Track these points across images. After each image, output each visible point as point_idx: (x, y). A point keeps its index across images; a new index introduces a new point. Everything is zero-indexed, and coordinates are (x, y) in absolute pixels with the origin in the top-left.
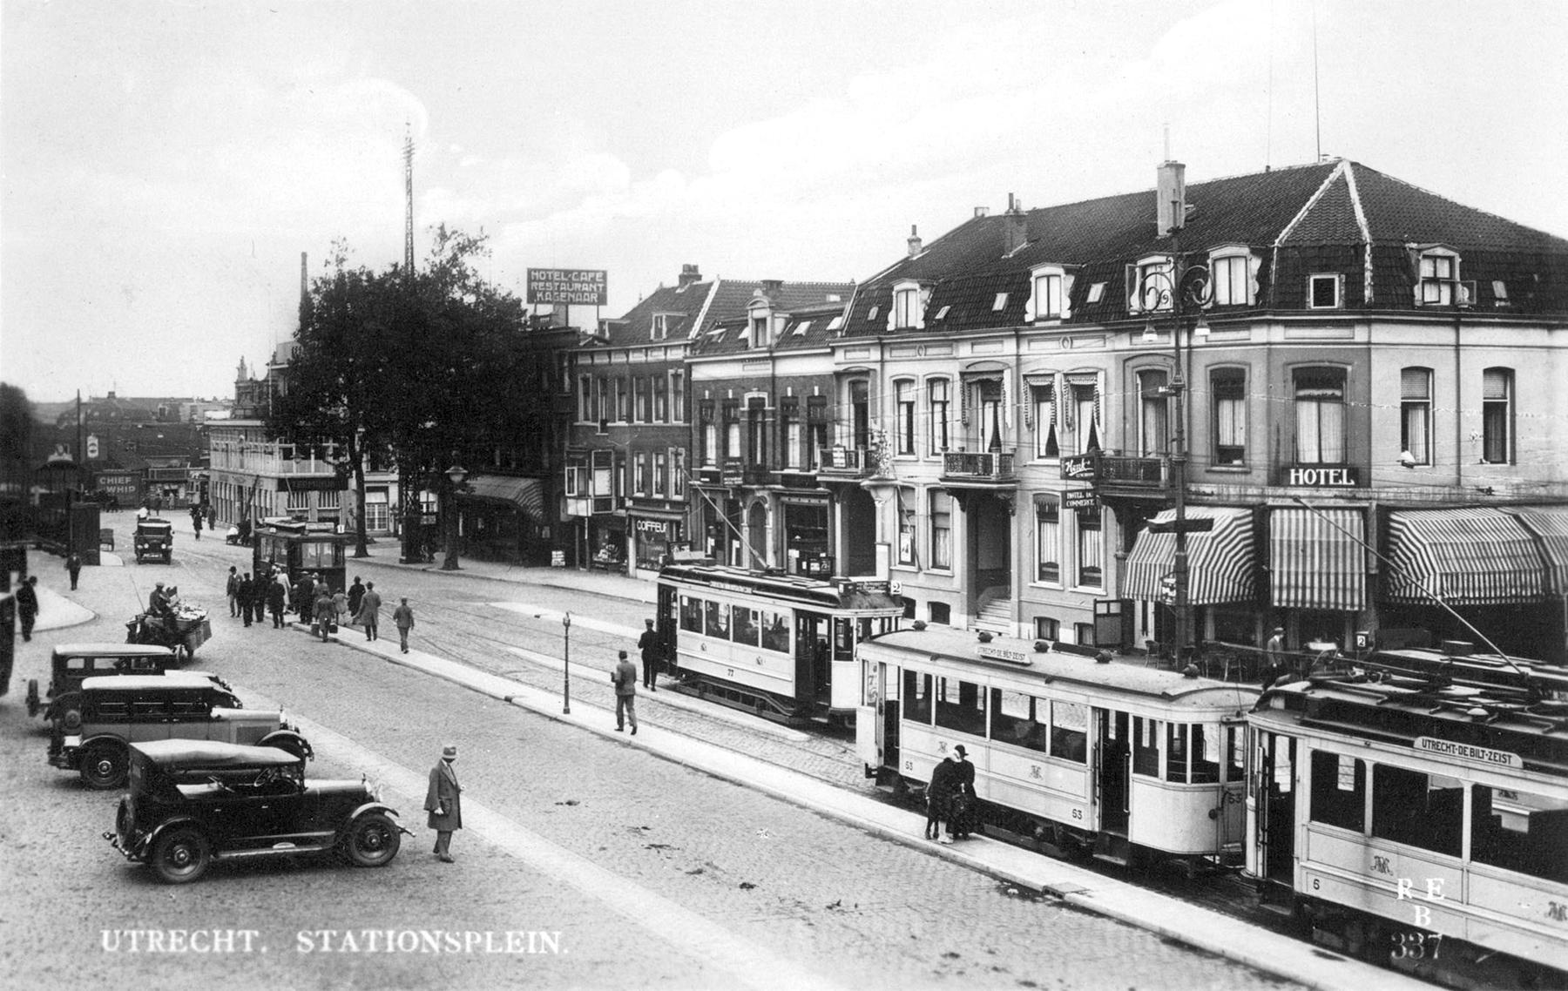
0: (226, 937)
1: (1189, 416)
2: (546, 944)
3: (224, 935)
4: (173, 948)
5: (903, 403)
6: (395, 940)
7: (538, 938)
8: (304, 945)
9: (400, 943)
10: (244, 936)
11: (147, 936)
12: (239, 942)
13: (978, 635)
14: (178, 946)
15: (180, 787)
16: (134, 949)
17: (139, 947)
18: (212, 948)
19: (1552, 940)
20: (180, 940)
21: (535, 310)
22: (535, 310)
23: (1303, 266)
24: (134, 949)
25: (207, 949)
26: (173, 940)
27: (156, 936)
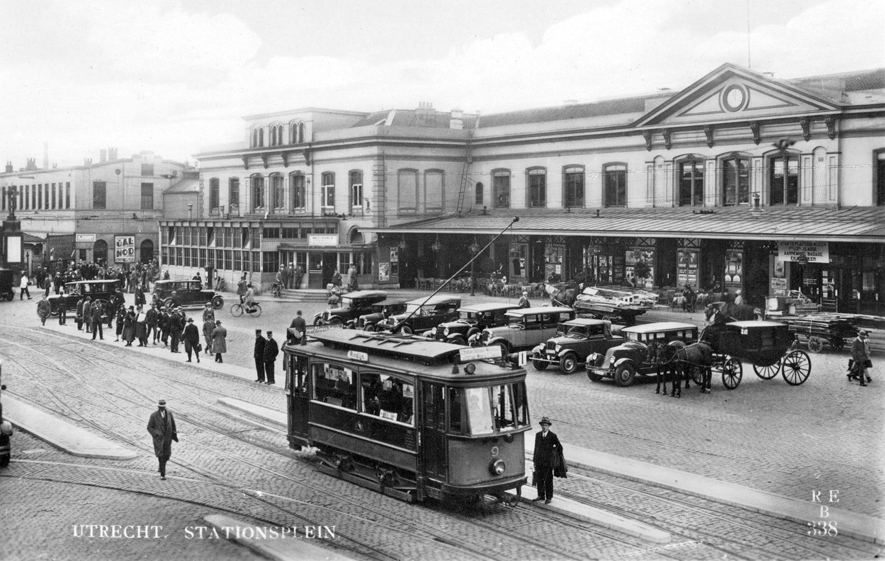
0: (144, 530)
1: (409, 139)
2: (259, 533)
3: (143, 528)
4: (113, 536)
5: (351, 209)
6: (241, 532)
7: (323, 528)
8: (188, 535)
9: (244, 533)
10: (89, 528)
11: (99, 529)
12: (152, 533)
13: (296, 316)
14: (116, 534)
15: (522, 407)
16: (92, 535)
17: (159, 535)
18: (136, 536)
19: (850, 535)
20: (118, 531)
21: (391, 201)
22: (391, 201)
23: (96, 293)
24: (92, 535)
25: (133, 536)
26: (114, 531)
27: (104, 529)
